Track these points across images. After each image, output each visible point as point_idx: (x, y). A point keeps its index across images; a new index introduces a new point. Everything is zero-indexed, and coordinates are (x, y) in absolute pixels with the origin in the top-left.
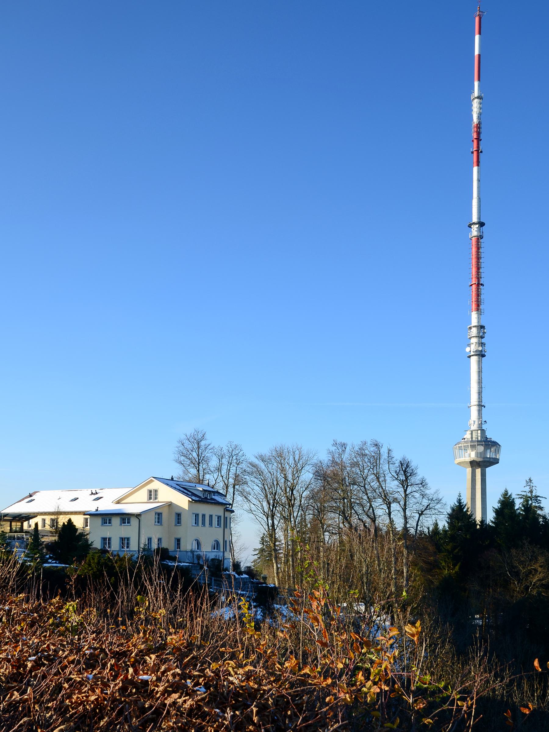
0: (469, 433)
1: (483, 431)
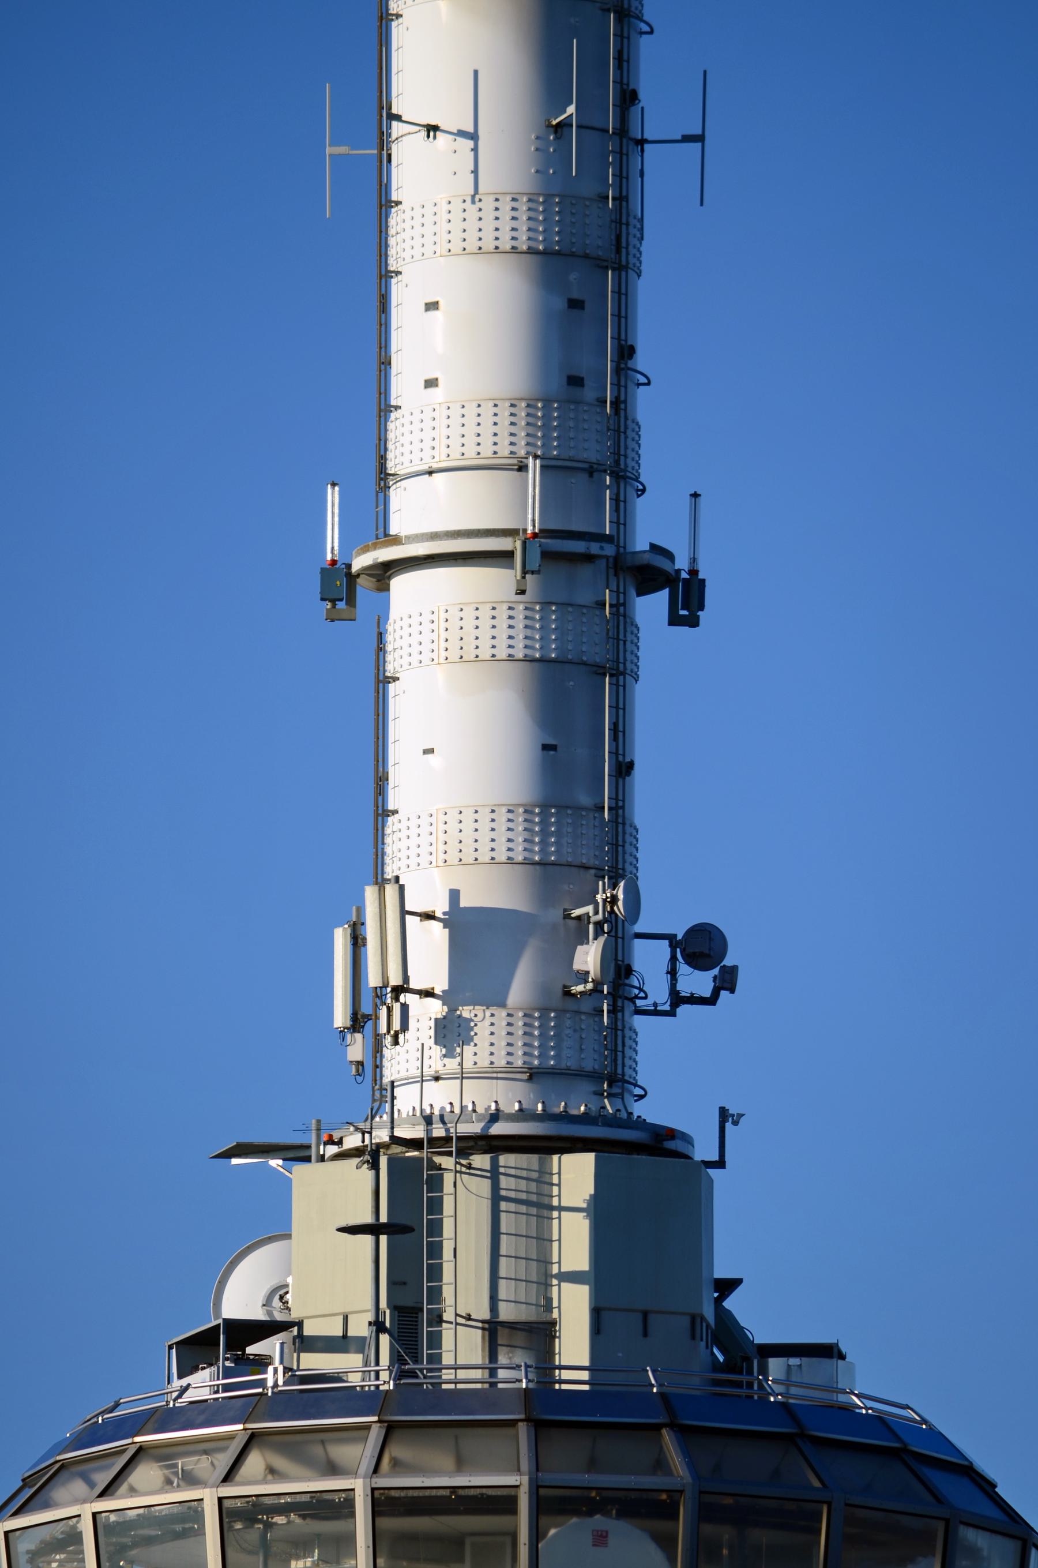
0: (337, 1193)
1: (656, 1178)
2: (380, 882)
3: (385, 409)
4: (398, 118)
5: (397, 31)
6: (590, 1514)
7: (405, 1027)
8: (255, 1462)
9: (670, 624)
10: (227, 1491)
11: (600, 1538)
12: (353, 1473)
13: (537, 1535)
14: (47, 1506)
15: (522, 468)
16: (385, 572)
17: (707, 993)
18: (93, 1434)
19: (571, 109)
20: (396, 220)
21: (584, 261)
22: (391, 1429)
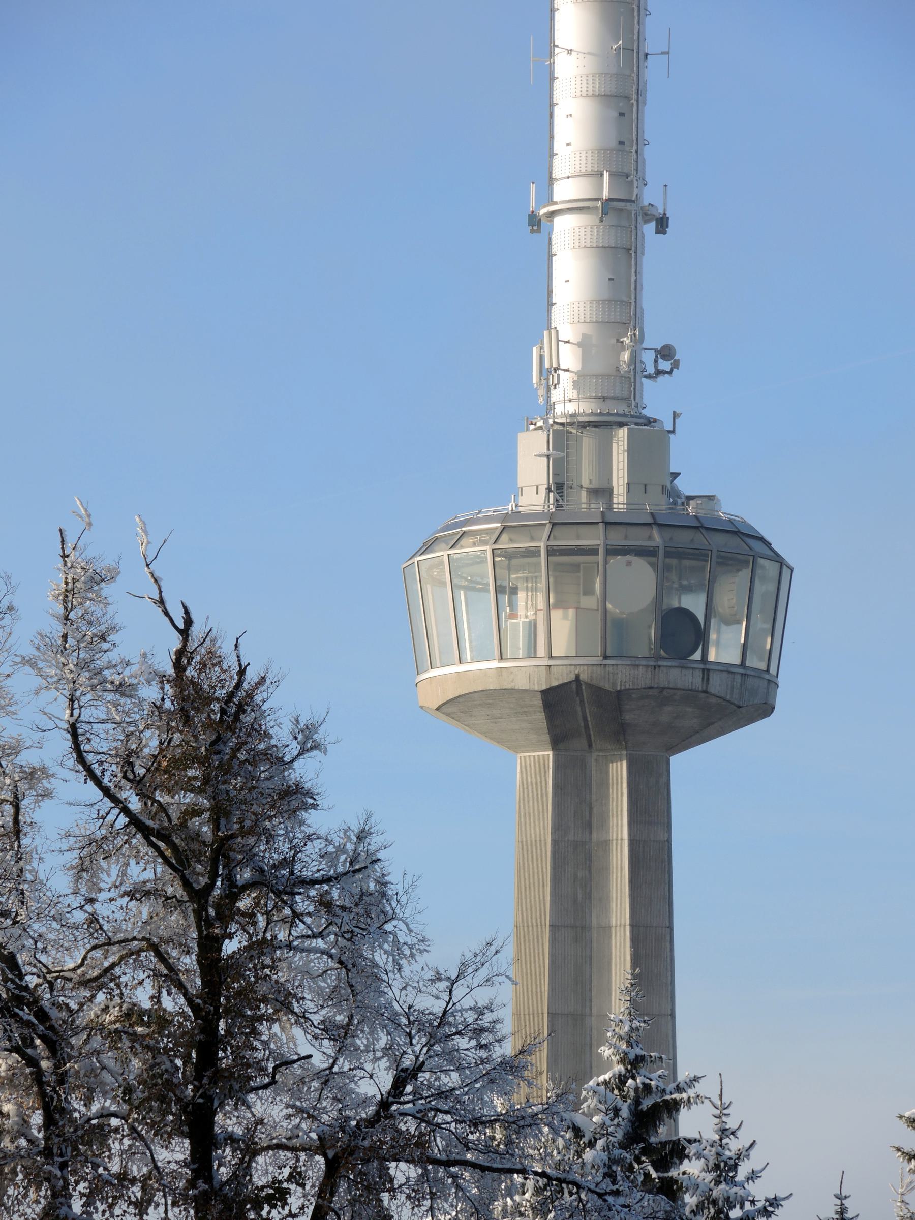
1: (651, 439)
2: (549, 328)
3: (552, 155)
4: (557, 46)
5: (557, 15)
6: (625, 554)
7: (558, 382)
8: (505, 537)
9: (657, 233)
10: (495, 547)
11: (629, 563)
12: (540, 540)
13: (606, 563)
14: (431, 552)
15: (602, 175)
16: (552, 214)
17: (669, 370)
18: (447, 528)
19: (620, 42)
20: (556, 84)
21: (623, 99)
22: (554, 524)
